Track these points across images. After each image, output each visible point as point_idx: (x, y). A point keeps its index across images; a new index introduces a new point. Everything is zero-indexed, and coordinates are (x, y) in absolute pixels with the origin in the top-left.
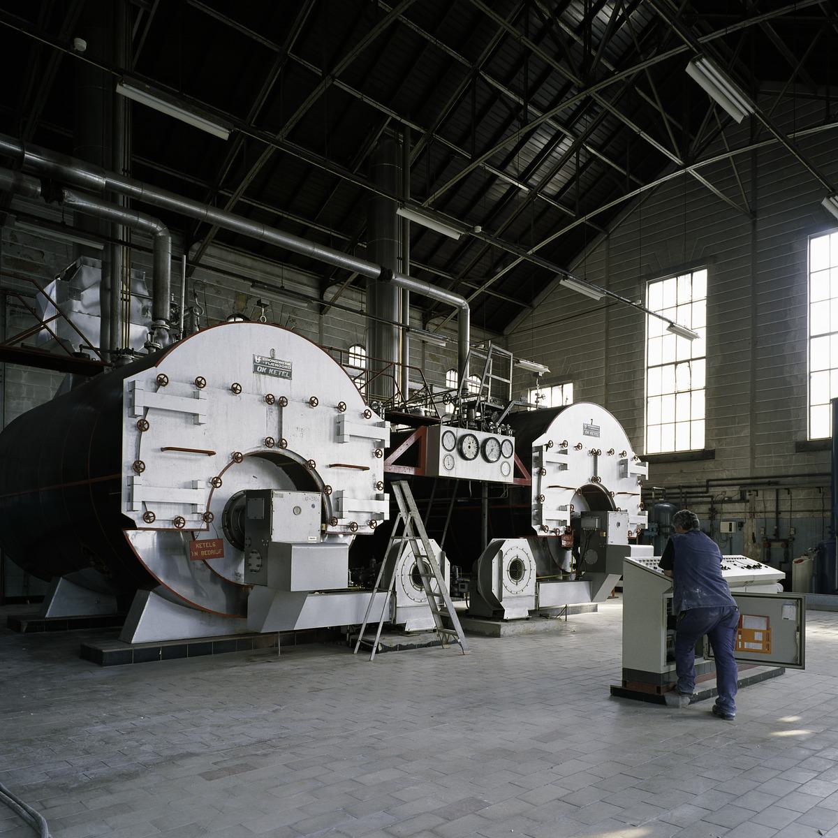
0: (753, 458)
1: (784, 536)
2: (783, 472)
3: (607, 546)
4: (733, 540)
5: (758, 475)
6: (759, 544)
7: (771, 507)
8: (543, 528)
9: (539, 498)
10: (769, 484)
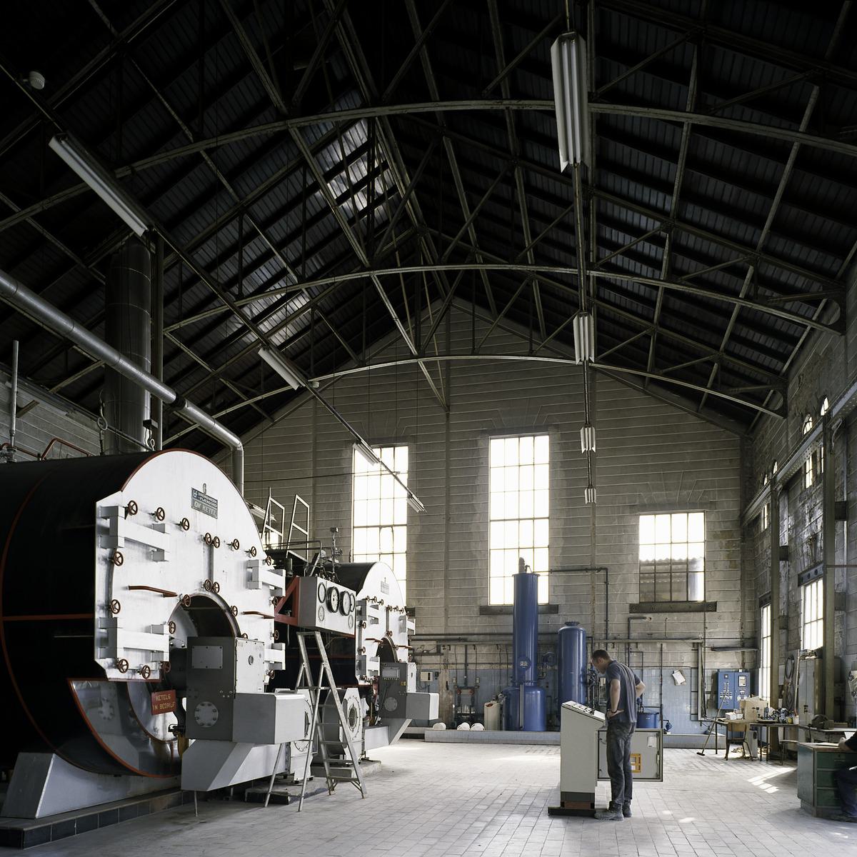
0: (447, 618)
1: (471, 684)
2: (471, 631)
3: (235, 695)
4: (430, 687)
5: (451, 632)
6: (452, 691)
7: (461, 659)
8: (118, 665)
9: (110, 607)
10: (459, 640)
